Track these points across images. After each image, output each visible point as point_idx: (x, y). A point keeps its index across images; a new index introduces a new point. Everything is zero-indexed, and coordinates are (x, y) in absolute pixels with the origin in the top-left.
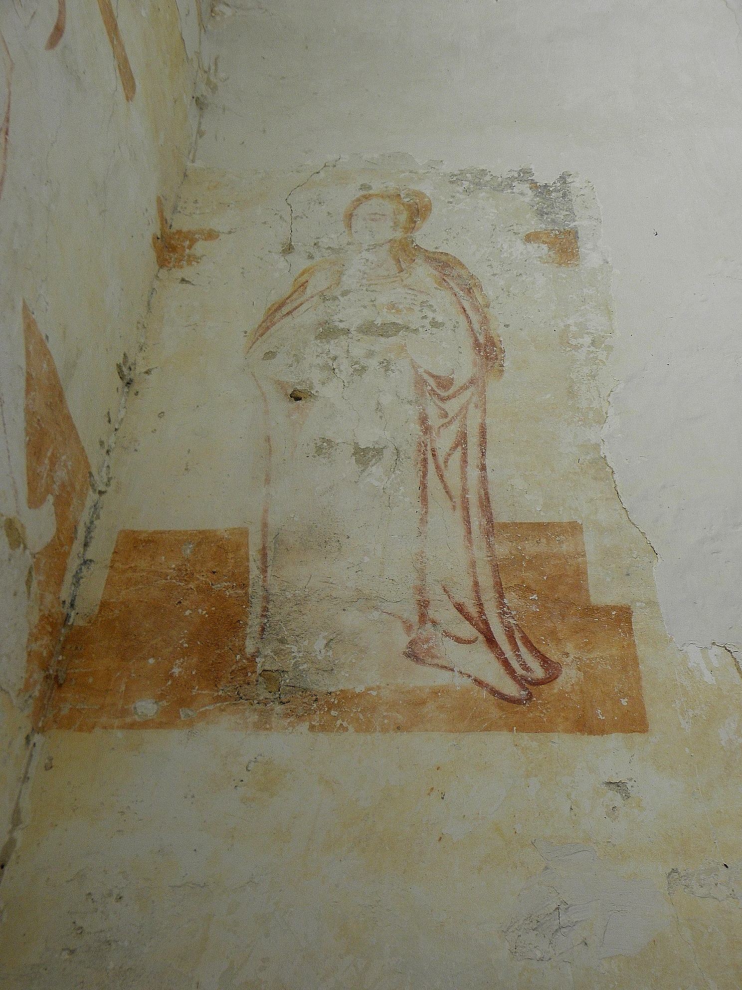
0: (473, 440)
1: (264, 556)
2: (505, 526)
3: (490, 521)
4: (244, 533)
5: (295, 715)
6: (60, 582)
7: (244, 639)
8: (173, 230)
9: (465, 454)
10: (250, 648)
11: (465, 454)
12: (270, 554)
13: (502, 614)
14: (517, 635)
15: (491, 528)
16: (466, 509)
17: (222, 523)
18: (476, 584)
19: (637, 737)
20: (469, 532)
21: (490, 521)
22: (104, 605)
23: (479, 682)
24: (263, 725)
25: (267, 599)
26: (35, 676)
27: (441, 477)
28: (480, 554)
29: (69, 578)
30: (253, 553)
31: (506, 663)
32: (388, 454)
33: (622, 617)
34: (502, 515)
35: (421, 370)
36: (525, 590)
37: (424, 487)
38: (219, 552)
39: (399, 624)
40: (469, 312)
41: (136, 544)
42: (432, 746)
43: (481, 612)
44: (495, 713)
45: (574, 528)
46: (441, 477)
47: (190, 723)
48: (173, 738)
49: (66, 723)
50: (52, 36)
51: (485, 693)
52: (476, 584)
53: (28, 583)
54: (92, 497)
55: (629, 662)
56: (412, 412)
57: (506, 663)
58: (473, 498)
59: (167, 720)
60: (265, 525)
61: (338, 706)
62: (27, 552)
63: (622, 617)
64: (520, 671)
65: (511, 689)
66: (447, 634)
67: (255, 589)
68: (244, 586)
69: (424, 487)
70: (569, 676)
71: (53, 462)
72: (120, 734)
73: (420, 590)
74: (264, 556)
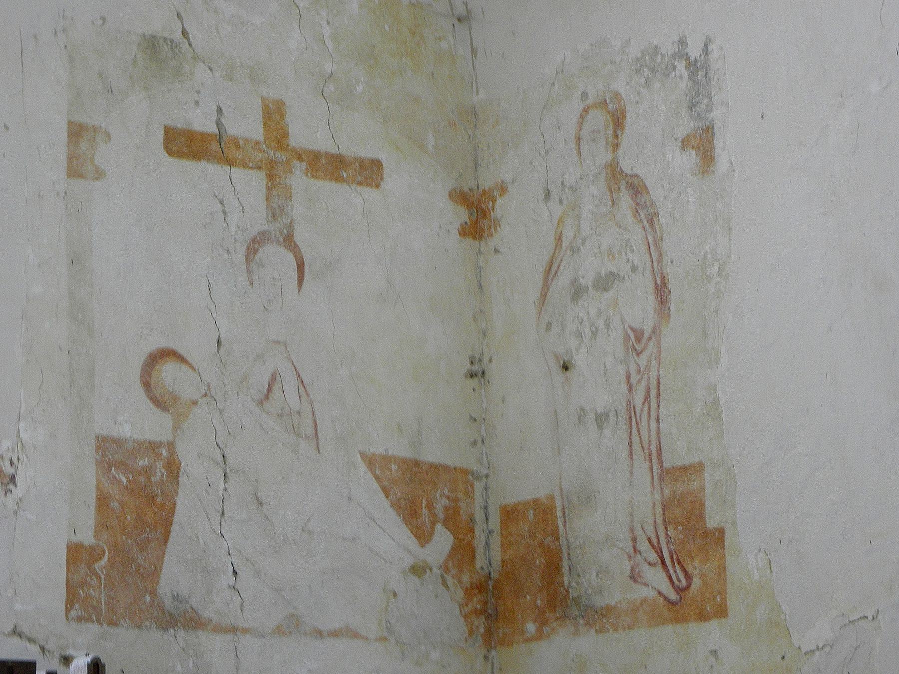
0: (653, 393)
1: (564, 513)
2: (669, 470)
3: (662, 467)
4: (552, 498)
5: (589, 624)
6: (473, 557)
7: (563, 577)
8: (468, 221)
9: (649, 408)
10: (566, 584)
11: (649, 408)
12: (566, 511)
13: (668, 542)
14: (675, 557)
15: (664, 473)
16: (651, 459)
17: (541, 493)
18: (655, 521)
19: (723, 620)
20: (653, 479)
21: (662, 467)
22: (504, 563)
23: (660, 593)
24: (576, 633)
25: (569, 547)
26: (476, 623)
27: (639, 432)
28: (658, 496)
29: (480, 551)
30: (559, 513)
31: (670, 578)
32: (612, 416)
33: (719, 536)
34: (667, 464)
35: (626, 325)
36: (677, 523)
37: (630, 443)
38: (543, 511)
39: (626, 556)
40: (651, 247)
41: (510, 514)
42: (641, 636)
43: (659, 543)
44: (666, 613)
45: (699, 468)
46: (639, 432)
47: (548, 636)
48: (543, 644)
49: (505, 642)
50: (299, 277)
51: (662, 600)
52: (655, 521)
53: (445, 584)
54: (478, 486)
55: (721, 570)
56: (621, 370)
57: (670, 578)
58: (654, 448)
59: (539, 636)
60: (561, 488)
61: (603, 616)
62: (435, 570)
63: (719, 536)
64: (676, 582)
65: (673, 596)
66: (646, 560)
67: (563, 541)
68: (558, 539)
69: (630, 443)
70: (696, 582)
71: (430, 507)
72: (523, 646)
73: (632, 530)
74: (564, 513)
